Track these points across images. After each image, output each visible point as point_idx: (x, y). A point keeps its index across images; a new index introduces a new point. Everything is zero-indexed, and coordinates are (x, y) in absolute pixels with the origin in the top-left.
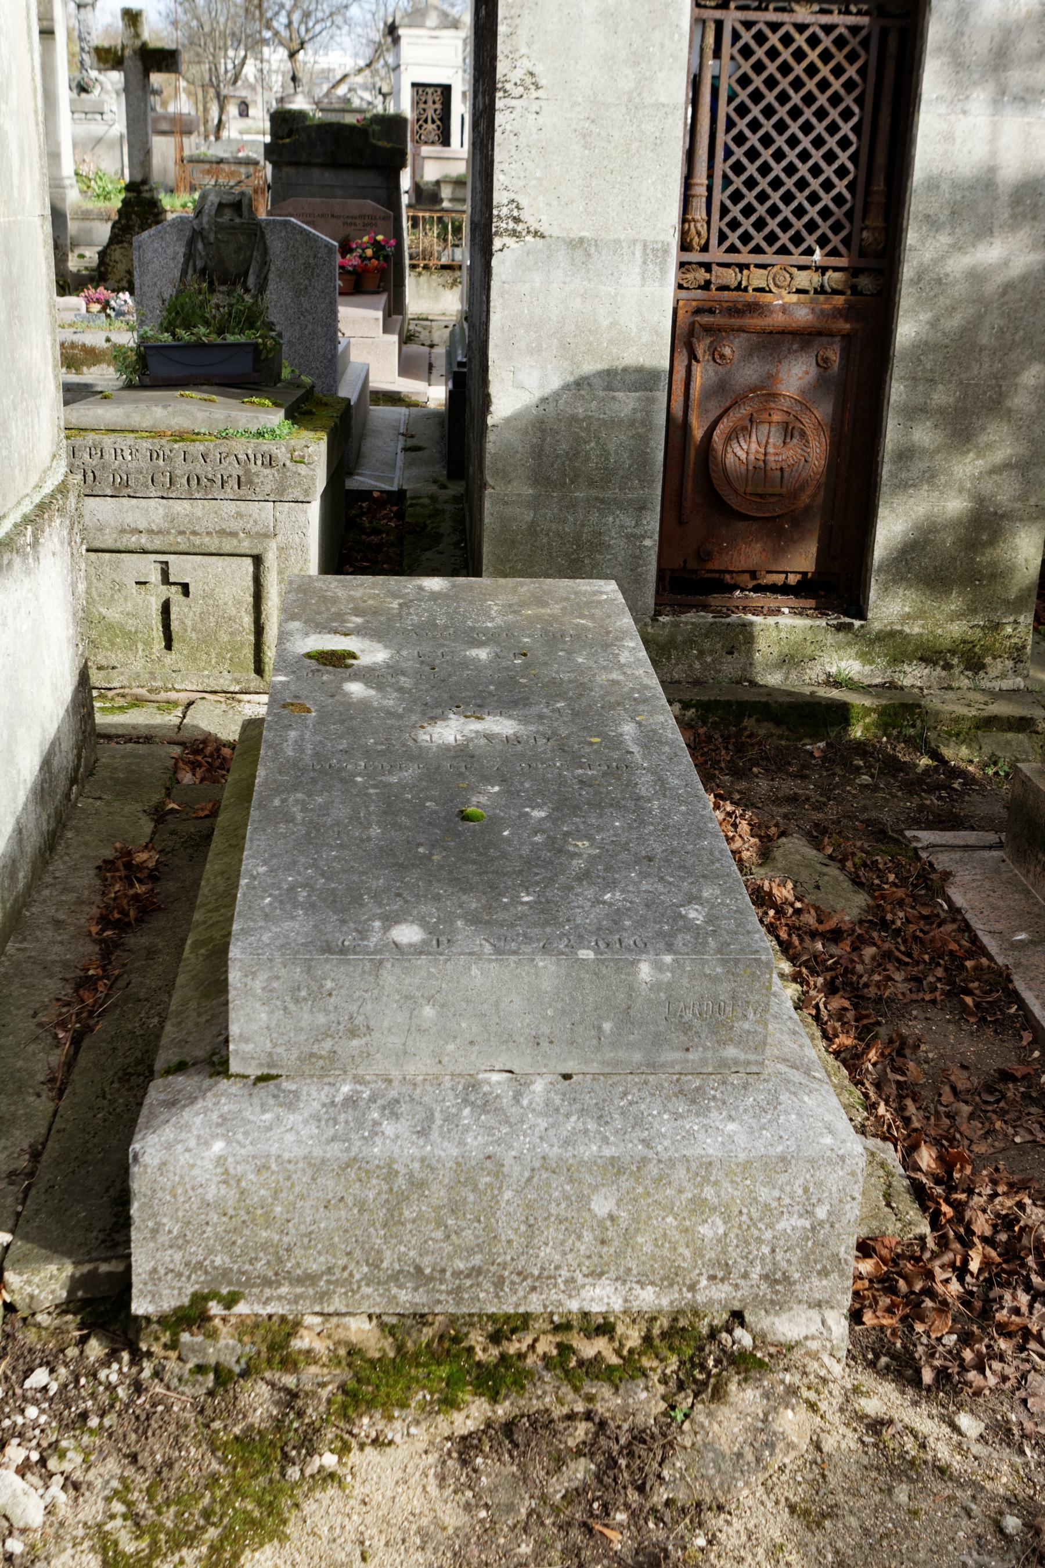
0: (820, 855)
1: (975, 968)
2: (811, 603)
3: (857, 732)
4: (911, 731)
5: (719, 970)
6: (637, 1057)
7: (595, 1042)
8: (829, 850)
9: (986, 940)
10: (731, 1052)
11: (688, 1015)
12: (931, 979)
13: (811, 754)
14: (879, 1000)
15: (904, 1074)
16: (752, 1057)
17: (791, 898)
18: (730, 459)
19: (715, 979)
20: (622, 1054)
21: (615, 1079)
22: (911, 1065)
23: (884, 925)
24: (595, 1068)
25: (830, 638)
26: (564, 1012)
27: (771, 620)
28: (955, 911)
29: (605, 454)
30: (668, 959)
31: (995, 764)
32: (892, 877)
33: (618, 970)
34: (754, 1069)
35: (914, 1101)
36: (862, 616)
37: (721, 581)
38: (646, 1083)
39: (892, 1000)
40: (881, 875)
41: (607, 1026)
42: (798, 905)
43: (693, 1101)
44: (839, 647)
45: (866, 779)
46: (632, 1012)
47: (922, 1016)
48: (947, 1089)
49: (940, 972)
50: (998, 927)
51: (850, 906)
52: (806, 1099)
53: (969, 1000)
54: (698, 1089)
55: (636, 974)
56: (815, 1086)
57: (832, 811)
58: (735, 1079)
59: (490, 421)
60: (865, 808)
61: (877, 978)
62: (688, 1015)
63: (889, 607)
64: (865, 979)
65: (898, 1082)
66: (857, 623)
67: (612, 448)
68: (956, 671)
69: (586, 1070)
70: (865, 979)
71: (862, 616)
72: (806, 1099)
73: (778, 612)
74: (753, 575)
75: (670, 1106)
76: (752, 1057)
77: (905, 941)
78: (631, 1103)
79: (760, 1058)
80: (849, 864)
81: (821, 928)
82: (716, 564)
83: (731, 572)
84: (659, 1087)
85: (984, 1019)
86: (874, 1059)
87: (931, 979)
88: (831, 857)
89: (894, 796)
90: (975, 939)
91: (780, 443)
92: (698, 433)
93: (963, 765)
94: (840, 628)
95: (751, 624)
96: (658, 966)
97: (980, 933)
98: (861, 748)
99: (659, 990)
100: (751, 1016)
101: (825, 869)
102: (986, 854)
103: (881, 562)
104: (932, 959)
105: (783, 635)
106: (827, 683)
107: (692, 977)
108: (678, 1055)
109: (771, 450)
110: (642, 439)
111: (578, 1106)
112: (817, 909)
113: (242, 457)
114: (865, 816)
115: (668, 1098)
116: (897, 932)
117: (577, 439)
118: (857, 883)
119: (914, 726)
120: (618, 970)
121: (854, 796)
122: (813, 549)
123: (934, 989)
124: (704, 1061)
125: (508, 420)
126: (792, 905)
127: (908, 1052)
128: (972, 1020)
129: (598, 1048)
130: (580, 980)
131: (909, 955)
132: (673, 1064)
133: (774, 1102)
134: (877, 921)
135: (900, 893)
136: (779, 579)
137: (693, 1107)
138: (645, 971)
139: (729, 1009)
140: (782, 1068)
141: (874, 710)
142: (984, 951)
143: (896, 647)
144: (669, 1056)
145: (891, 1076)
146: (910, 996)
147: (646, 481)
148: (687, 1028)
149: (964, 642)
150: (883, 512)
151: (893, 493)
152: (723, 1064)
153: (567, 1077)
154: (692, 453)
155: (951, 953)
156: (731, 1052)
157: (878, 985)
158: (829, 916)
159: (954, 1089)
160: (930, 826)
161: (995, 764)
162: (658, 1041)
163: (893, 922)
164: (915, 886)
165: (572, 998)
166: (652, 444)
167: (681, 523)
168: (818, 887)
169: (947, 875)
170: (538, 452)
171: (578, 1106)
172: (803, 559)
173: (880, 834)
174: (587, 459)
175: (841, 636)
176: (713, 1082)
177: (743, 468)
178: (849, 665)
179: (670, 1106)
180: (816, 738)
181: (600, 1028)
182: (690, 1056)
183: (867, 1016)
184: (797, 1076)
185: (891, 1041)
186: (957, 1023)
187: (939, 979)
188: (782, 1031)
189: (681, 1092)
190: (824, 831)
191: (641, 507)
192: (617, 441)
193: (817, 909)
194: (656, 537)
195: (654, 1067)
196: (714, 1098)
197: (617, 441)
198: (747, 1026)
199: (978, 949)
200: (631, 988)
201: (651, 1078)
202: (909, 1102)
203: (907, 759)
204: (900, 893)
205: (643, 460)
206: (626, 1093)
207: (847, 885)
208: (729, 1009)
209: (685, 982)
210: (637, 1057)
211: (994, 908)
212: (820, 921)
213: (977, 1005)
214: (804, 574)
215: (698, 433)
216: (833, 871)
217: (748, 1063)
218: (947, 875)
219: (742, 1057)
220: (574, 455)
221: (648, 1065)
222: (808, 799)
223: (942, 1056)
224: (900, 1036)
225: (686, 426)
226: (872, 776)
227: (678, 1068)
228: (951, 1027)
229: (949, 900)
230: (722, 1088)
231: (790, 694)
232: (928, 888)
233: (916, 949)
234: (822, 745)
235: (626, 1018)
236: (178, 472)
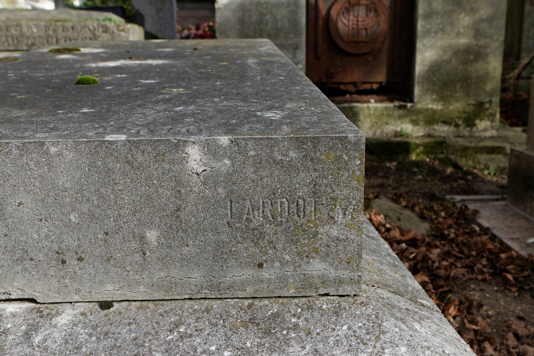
0: (399, 206)
1: (507, 258)
2: (385, 98)
3: (413, 157)
4: (441, 156)
5: (293, 154)
6: (196, 276)
7: (138, 257)
8: (404, 204)
9: (510, 243)
10: (317, 267)
11: (258, 219)
12: (479, 266)
13: (390, 168)
14: (447, 278)
15: (476, 325)
16: (345, 274)
17: (383, 221)
18: (340, 25)
19: (288, 168)
20: (175, 273)
21: (168, 306)
22: (479, 319)
23: (443, 237)
24: (141, 292)
25: (397, 113)
26: (92, 216)
27: (365, 105)
28: (485, 231)
29: (276, 21)
30: (224, 140)
31: (488, 169)
32: (443, 214)
33: (159, 157)
34: (348, 289)
35: (491, 344)
36: (412, 101)
37: (339, 89)
38: (207, 310)
39: (455, 278)
40: (437, 213)
41: (152, 235)
42: (388, 226)
43: (268, 332)
44: (400, 117)
45: (420, 177)
46: (183, 215)
47: (477, 288)
48: (510, 335)
49: (484, 261)
50: (515, 236)
51: (421, 229)
52: (417, 326)
53: (509, 277)
54: (275, 316)
55: (185, 159)
56: (425, 313)
57: (403, 190)
58: (324, 304)
59: (217, 6)
60: (421, 189)
61: (445, 263)
62: (258, 219)
63: (424, 100)
64: (436, 264)
65: (474, 330)
66: (409, 105)
67: (279, 17)
68: (461, 128)
69: (130, 296)
70: (436, 264)
71: (412, 101)
72: (417, 326)
73: (368, 102)
74: (354, 84)
75: (235, 340)
76: (345, 274)
77: (457, 245)
78: (182, 337)
79: (355, 275)
80: (417, 209)
81: (403, 238)
82: (335, 80)
83: (344, 84)
84: (225, 315)
85: (523, 289)
86: (454, 313)
87: (479, 266)
88: (406, 207)
89: (436, 184)
90: (502, 243)
91: (364, 15)
92: (323, 12)
93: (471, 169)
94: (400, 107)
95: (355, 107)
96: (212, 151)
97: (505, 240)
98: (416, 164)
99: (216, 184)
100: (340, 218)
101: (403, 212)
102: (496, 203)
103: (419, 76)
104: (478, 254)
105: (372, 112)
106: (396, 136)
107: (258, 164)
108: (248, 273)
109: (360, 19)
110: (294, 12)
111: (109, 342)
112: (400, 229)
113: (92, 28)
114: (422, 191)
115: (234, 329)
116: (452, 241)
117: (262, 14)
118: (422, 217)
119: (442, 153)
120: (159, 157)
121: (415, 184)
122: (384, 71)
123: (482, 273)
124: (283, 281)
125: (226, 5)
126: (384, 226)
127: (474, 311)
128: (514, 289)
129: (144, 266)
130: (110, 171)
131: (462, 252)
132: (243, 285)
133: (376, 330)
134: (438, 234)
135: (450, 221)
136: (368, 86)
137: (267, 341)
138: (195, 157)
139: (310, 209)
140: (385, 293)
141: (421, 145)
142: (509, 249)
143: (431, 119)
144: (238, 274)
145: (468, 325)
146: (468, 276)
147: (297, 34)
148: (257, 236)
149: (465, 112)
150: (419, 45)
151: (424, 36)
152: (307, 283)
153: (105, 305)
154: (320, 22)
155: (490, 250)
156: (317, 267)
157: (446, 268)
158: (409, 231)
159: (517, 336)
160: (459, 194)
161: (488, 169)
162: (221, 254)
163: (449, 235)
164: (458, 218)
165: (101, 197)
166: (300, 15)
167: (317, 58)
168: (399, 219)
169: (476, 212)
170: (242, 22)
171: (109, 342)
172: (380, 77)
173: (432, 197)
174: (267, 24)
175: (401, 112)
176: (294, 306)
177: (346, 29)
178: (407, 127)
179: (235, 340)
180: (391, 160)
181: (142, 238)
182: (265, 274)
183: (442, 286)
184: (403, 303)
185: (461, 303)
186: (501, 292)
187: (484, 266)
188: (381, 263)
189: (252, 320)
190: (401, 196)
191: (296, 48)
192: (282, 14)
193: (400, 229)
194: (304, 63)
195: (219, 292)
196: (296, 326)
197: (282, 14)
198: (335, 233)
199: (506, 249)
200: (179, 183)
201: (215, 304)
202: (487, 345)
203: (441, 168)
204: (450, 221)
205: (295, 23)
206: (177, 325)
207: (416, 219)
208: (310, 209)
209: (249, 171)
210: (196, 276)
211: (510, 227)
212: (402, 234)
213: (516, 279)
214: (380, 83)
215: (323, 12)
216: (408, 212)
217: (340, 282)
218: (476, 212)
219: (332, 273)
220: (260, 22)
221: (211, 288)
222: (389, 185)
223: (498, 313)
224: (467, 299)
225: (316, 7)
226: (423, 176)
227: (250, 291)
228: (499, 295)
229: (480, 225)
230: (307, 314)
231: (377, 139)
232: (465, 219)
233: (465, 250)
234: (395, 163)
235: (176, 224)
236: (60, 37)
